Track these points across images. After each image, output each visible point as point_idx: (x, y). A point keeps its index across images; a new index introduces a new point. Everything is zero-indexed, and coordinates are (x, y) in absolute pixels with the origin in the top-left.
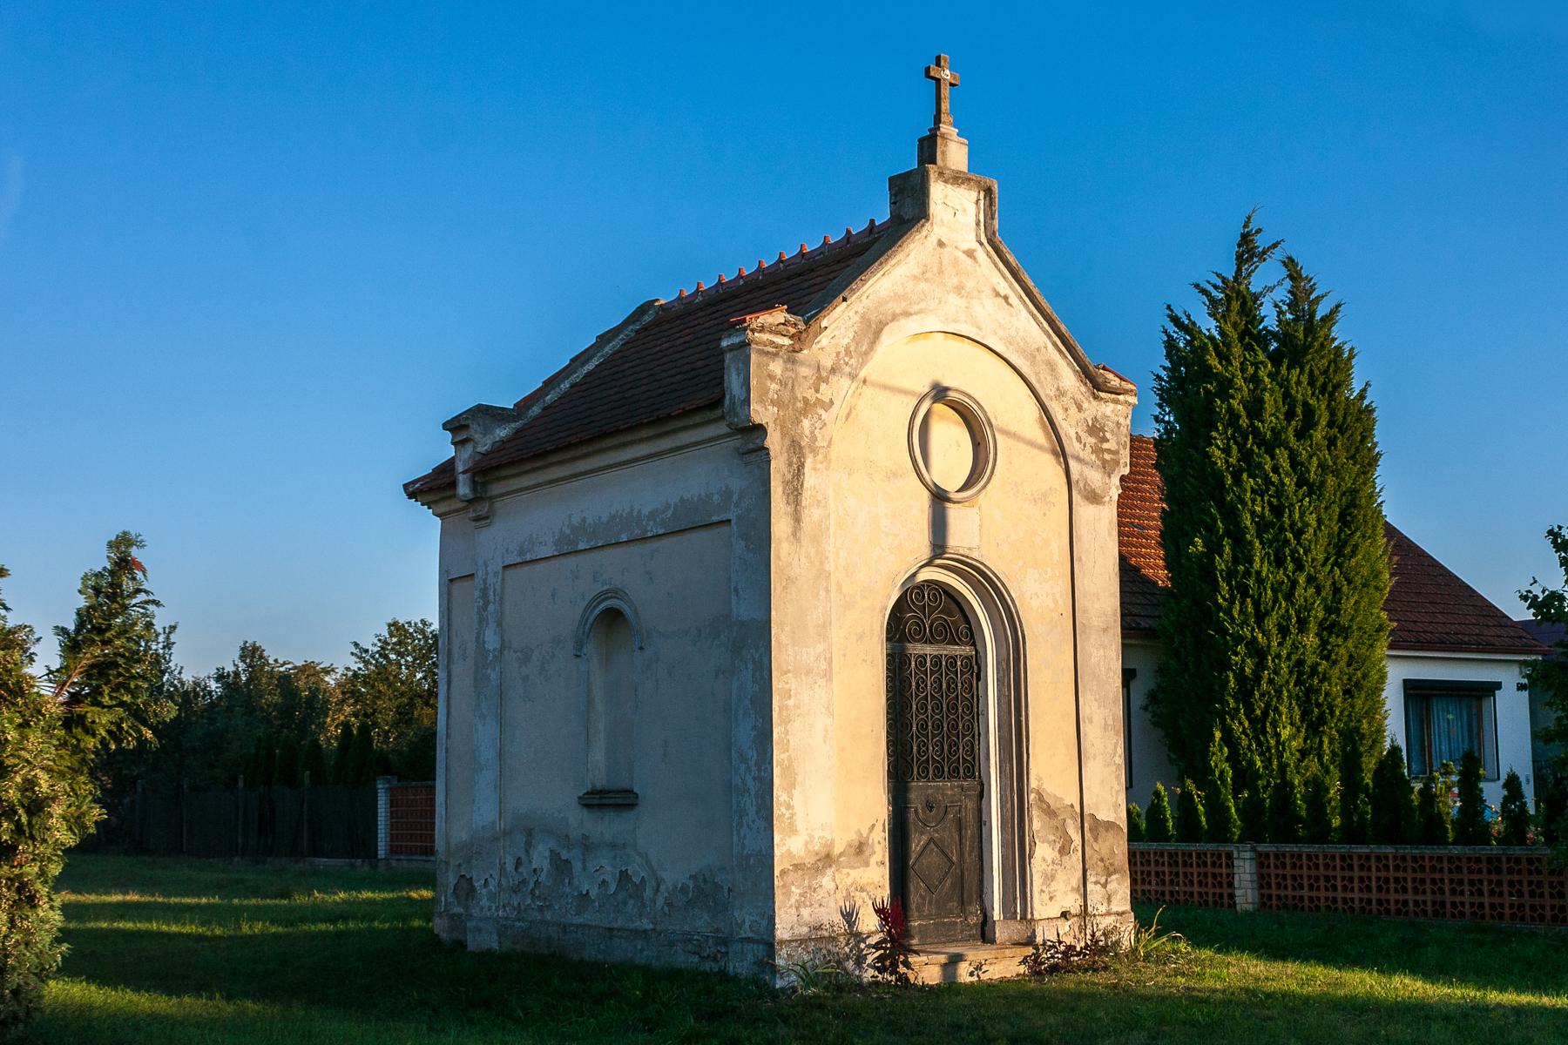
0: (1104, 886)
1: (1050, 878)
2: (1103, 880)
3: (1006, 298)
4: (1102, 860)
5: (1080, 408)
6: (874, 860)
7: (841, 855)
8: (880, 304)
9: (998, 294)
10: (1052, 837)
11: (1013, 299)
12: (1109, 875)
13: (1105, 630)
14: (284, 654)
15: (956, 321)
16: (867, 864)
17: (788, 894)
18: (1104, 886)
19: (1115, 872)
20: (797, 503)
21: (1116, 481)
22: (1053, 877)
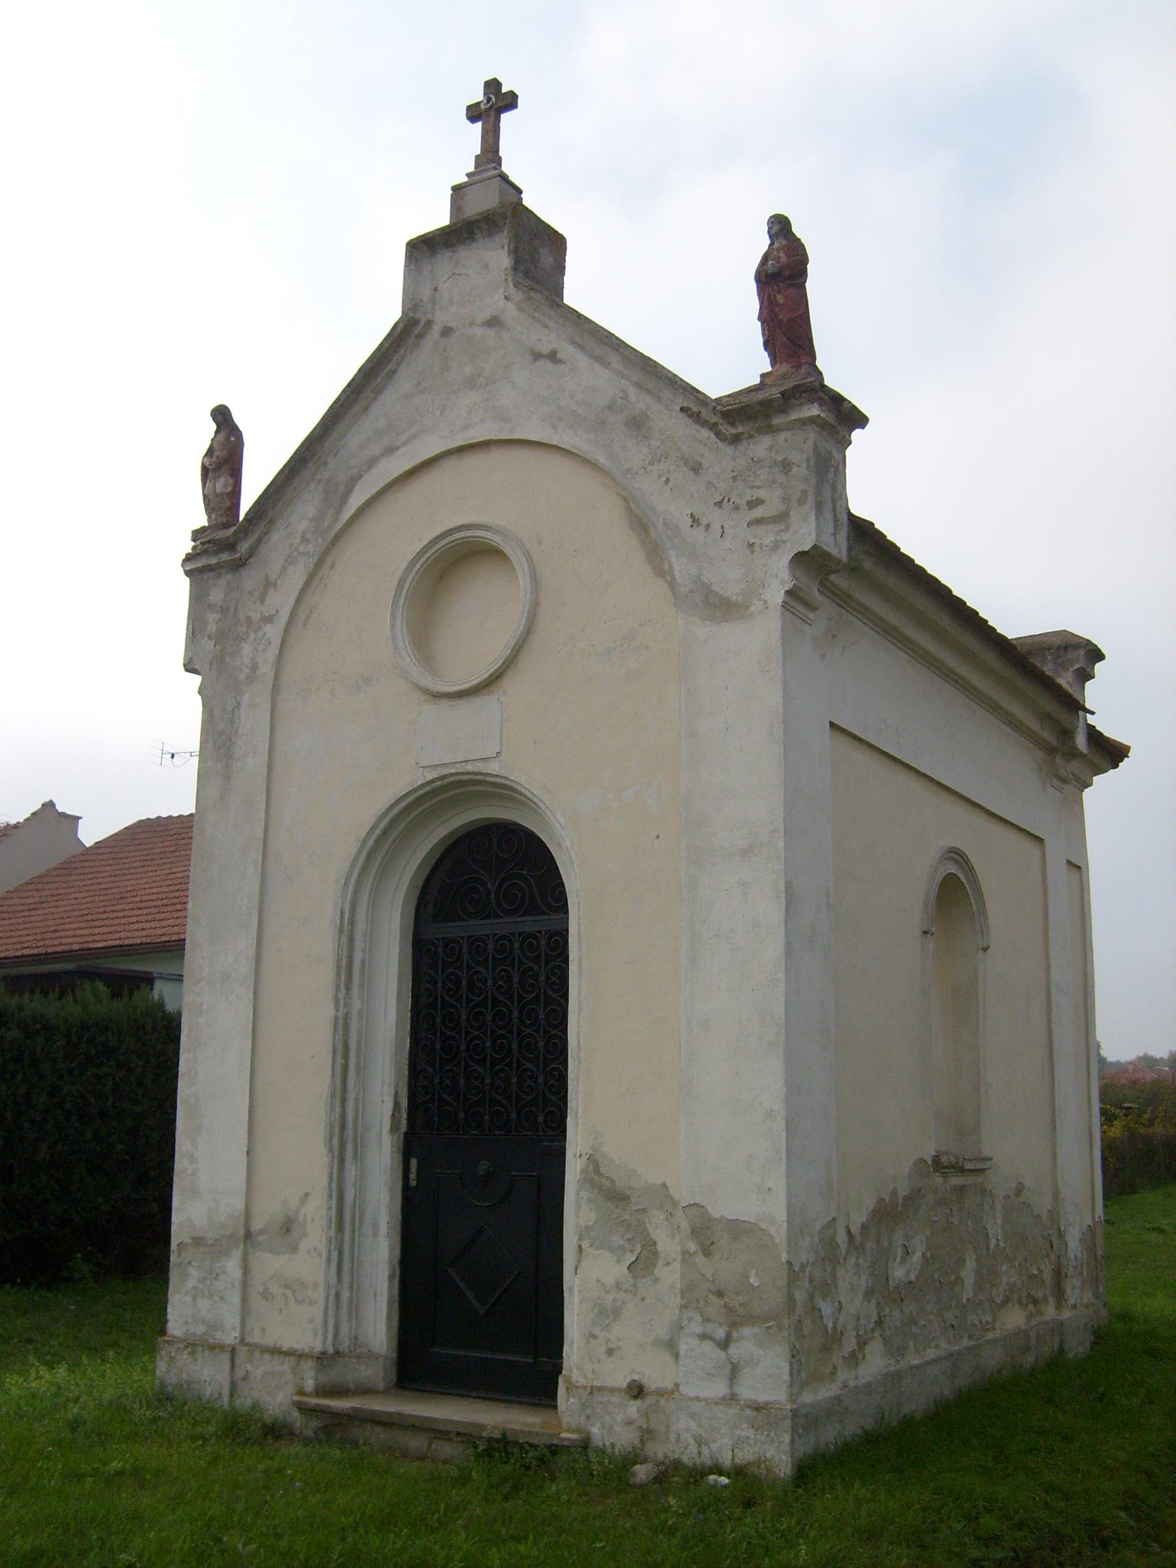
0: (724, 1344)
1: (608, 1314)
2: (720, 1333)
3: (553, 357)
4: (720, 1294)
5: (696, 469)
6: (304, 1245)
7: (262, 1231)
8: (620, 374)
9: (537, 356)
10: (617, 1240)
11: (567, 350)
12: (733, 1325)
13: (747, 852)
14: (1151, 1053)
15: (466, 427)
16: (294, 1249)
17: (185, 1277)
18: (724, 1344)
19: (751, 1320)
20: (229, 755)
21: (781, 563)
22: (616, 1314)
